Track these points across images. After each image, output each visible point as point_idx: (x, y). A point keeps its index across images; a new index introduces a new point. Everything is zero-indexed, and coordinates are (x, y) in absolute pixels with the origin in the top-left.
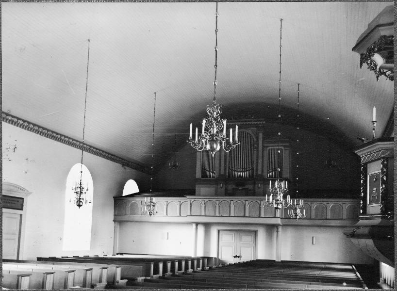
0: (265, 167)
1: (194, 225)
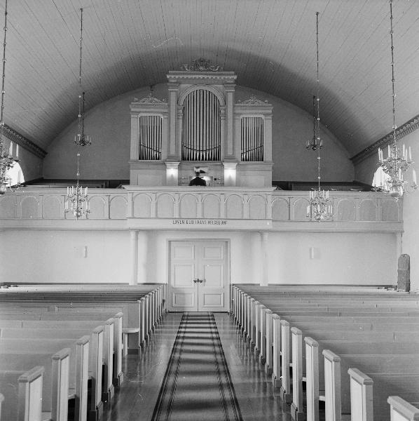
0: (171, 142)
1: (133, 234)
